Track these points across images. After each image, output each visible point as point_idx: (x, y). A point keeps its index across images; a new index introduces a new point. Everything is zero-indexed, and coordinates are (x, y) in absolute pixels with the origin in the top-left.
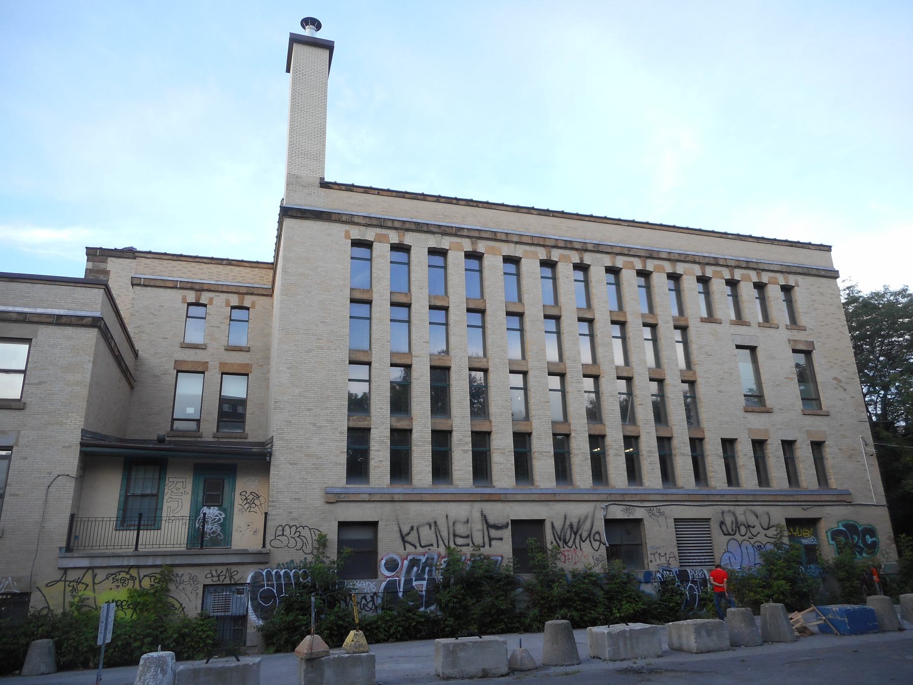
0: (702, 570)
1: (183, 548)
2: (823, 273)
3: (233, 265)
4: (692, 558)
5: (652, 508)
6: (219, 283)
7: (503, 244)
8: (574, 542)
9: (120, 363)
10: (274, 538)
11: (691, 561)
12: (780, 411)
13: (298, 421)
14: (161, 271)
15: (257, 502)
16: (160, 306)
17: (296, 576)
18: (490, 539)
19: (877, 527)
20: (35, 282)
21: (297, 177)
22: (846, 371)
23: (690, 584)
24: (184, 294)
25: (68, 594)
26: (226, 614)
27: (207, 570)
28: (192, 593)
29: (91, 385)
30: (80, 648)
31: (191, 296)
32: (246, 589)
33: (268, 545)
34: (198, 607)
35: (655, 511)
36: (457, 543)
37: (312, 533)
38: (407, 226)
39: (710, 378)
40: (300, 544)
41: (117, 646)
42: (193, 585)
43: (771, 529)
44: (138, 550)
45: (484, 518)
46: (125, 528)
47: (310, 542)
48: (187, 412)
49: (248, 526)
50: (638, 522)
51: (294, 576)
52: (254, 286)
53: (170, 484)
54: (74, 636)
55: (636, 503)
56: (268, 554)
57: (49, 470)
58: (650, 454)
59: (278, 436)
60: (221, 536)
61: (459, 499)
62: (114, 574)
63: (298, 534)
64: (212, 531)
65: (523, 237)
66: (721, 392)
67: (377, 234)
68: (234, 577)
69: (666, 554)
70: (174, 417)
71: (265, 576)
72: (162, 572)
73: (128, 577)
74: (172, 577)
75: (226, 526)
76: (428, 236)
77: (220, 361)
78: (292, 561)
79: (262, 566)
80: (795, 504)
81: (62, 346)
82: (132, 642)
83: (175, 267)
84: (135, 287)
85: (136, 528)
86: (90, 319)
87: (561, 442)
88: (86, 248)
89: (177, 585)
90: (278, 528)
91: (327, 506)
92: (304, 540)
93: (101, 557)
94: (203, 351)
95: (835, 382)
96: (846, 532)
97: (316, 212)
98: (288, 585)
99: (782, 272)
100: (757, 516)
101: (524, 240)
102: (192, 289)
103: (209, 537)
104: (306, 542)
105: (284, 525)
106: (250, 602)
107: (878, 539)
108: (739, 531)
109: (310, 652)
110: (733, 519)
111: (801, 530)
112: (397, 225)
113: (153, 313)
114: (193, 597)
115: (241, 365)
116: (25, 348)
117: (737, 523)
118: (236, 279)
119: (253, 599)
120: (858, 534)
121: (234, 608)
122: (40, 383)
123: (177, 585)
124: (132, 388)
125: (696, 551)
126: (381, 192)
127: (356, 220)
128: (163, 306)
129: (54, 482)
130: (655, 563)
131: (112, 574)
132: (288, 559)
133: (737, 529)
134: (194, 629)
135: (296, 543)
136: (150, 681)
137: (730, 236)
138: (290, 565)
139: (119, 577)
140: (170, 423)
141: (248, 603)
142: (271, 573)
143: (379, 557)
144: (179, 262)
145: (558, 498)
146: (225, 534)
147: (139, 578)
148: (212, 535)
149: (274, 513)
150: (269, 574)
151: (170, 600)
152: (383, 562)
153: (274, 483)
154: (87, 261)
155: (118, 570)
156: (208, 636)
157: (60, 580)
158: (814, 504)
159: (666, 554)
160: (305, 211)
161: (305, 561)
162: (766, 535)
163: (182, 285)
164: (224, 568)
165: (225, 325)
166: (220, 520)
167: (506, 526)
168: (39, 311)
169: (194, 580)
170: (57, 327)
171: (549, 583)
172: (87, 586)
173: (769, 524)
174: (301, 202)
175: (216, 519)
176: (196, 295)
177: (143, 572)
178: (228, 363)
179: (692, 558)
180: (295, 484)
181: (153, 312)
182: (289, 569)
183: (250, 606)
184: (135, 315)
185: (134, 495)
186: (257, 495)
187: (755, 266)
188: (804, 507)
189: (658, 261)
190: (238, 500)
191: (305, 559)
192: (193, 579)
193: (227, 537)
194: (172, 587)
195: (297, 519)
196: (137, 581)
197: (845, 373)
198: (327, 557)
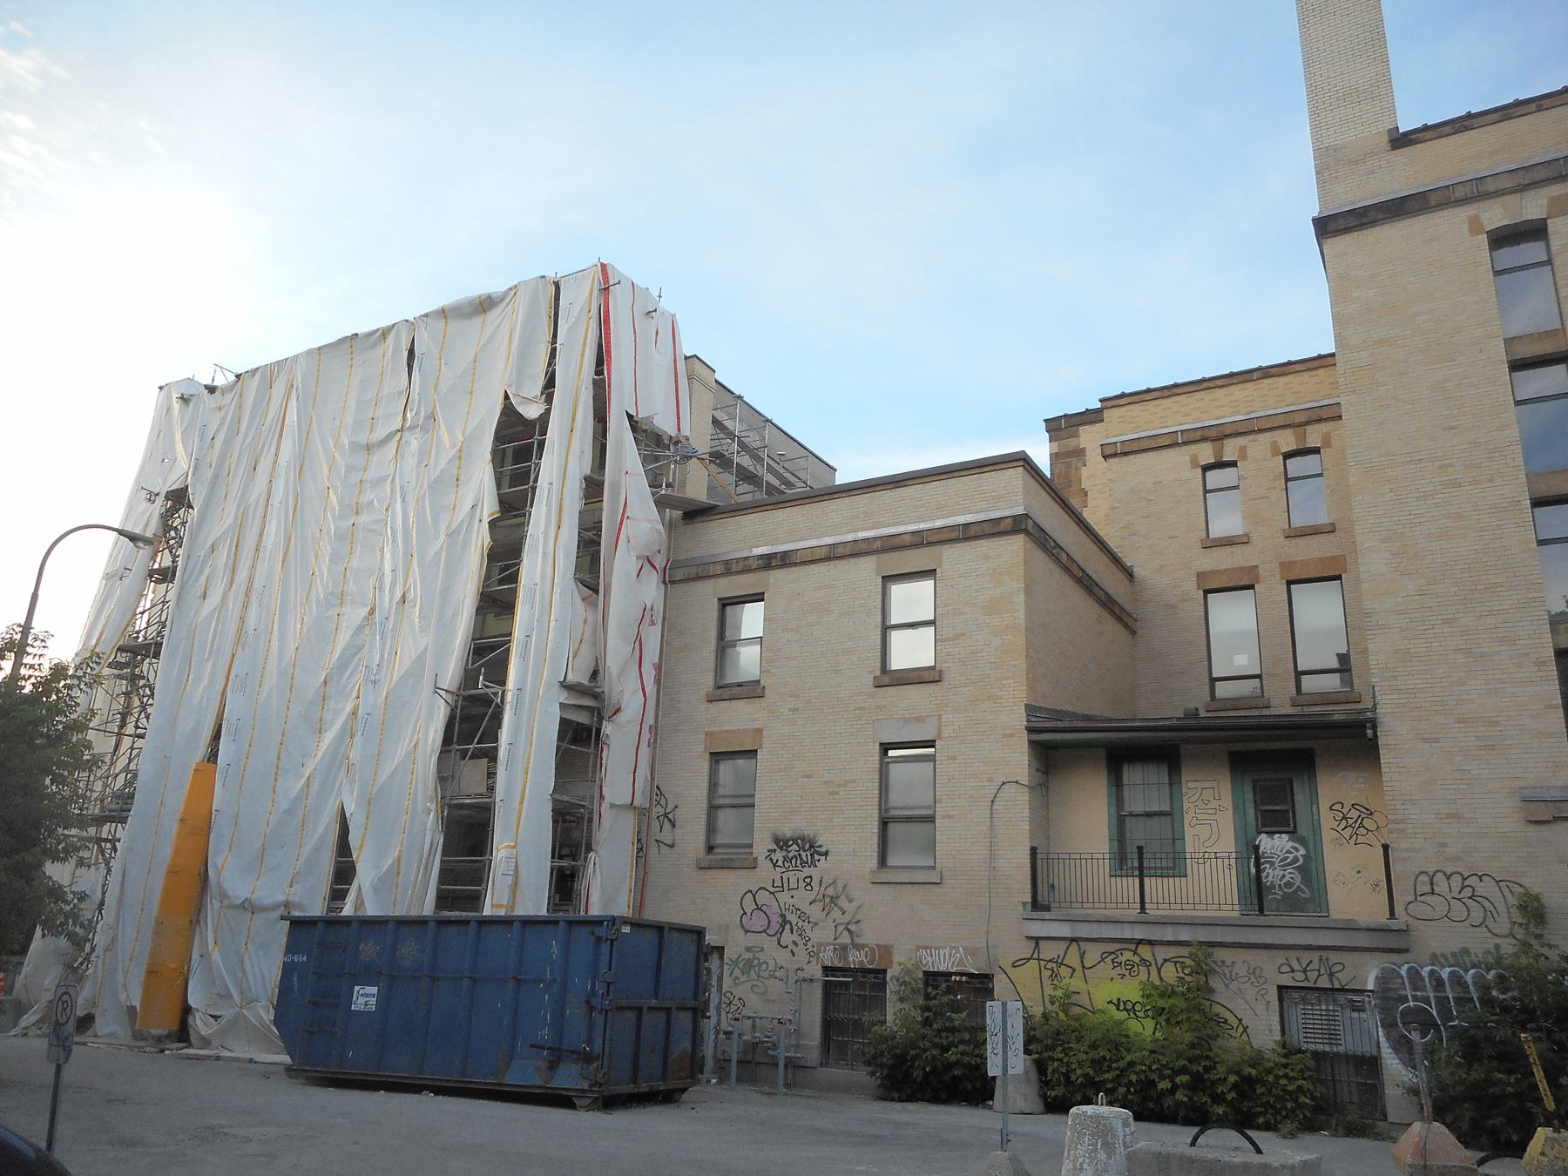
1: (1234, 913)
3: (1272, 376)
6: (1252, 416)
9: (1091, 591)
10: (1412, 898)
13: (1425, 650)
14: (1147, 423)
15: (1367, 823)
16: (1155, 483)
17: (1484, 988)
20: (927, 479)
21: (1335, 151)
24: (1192, 453)
25: (1047, 982)
26: (1335, 1050)
27: (1279, 957)
28: (1256, 1000)
29: (1028, 629)
30: (1073, 1078)
31: (1206, 454)
32: (1370, 1002)
33: (1399, 909)
34: (1274, 1028)
37: (1506, 890)
40: (1477, 915)
41: (1130, 1083)
42: (1256, 984)
44: (1147, 911)
46: (1124, 873)
47: (1502, 908)
48: (1236, 664)
49: (1359, 872)
51: (1475, 984)
52: (1320, 404)
53: (1191, 793)
54: (1061, 1056)
56: (1403, 932)
57: (988, 776)
59: (1387, 683)
60: (1304, 893)
62: (1113, 953)
63: (1467, 892)
64: (1284, 881)
67: (1551, 199)
68: (1338, 975)
70: (1214, 676)
71: (1406, 979)
72: (1191, 956)
73: (1136, 959)
74: (1213, 965)
75: (1311, 870)
77: (1280, 561)
78: (1465, 951)
79: (1395, 957)
81: (978, 573)
82: (1157, 1080)
83: (1169, 408)
84: (1112, 460)
85: (1136, 873)
86: (1010, 520)
88: (1045, 420)
89: (1227, 982)
90: (1420, 878)
91: (1532, 831)
92: (1487, 904)
93: (1171, 923)
94: (1244, 548)
97: (1390, 204)
98: (1463, 1001)
102: (1204, 439)
103: (1281, 893)
104: (1493, 910)
105: (1431, 870)
106: (1380, 1029)
109: (1422, 1163)
113: (1145, 498)
114: (1260, 1008)
115: (1321, 561)
116: (927, 586)
118: (1283, 401)
119: (1389, 1025)
121: (1349, 1038)
122: (957, 637)
123: (1227, 982)
124: (1133, 633)
126: (1546, 103)
127: (1491, 186)
128: (1161, 482)
129: (998, 795)
131: (1111, 953)
132: (1455, 946)
134: (1269, 1071)
135: (1469, 911)
136: (1084, 1161)
138: (1461, 958)
139: (1122, 959)
140: (1208, 686)
141: (1378, 1031)
142: (1417, 972)
144: (1174, 399)
146: (1310, 887)
147: (1156, 964)
148: (1286, 890)
149: (1404, 845)
150: (1414, 974)
151: (1217, 1009)
153: (1392, 783)
154: (1050, 442)
155: (1118, 946)
156: (1300, 1088)
157: (1031, 958)
160: (1366, 210)
161: (1498, 952)
163: (1186, 437)
164: (1315, 956)
165: (1277, 490)
166: (1296, 860)
168: (939, 523)
169: (1257, 975)
170: (967, 543)
172: (1074, 970)
174: (1356, 193)
175: (1287, 857)
176: (1214, 449)
177: (1163, 953)
178: (1296, 562)
180: (1441, 782)
181: (1144, 496)
182: (1460, 967)
183: (1383, 1040)
184: (1117, 508)
185: (1131, 815)
186: (1367, 810)
190: (1328, 821)
191: (1497, 947)
192: (1255, 973)
193: (1317, 895)
194: (1215, 983)
195: (1460, 859)
196: (1153, 969)
198: (1550, 947)
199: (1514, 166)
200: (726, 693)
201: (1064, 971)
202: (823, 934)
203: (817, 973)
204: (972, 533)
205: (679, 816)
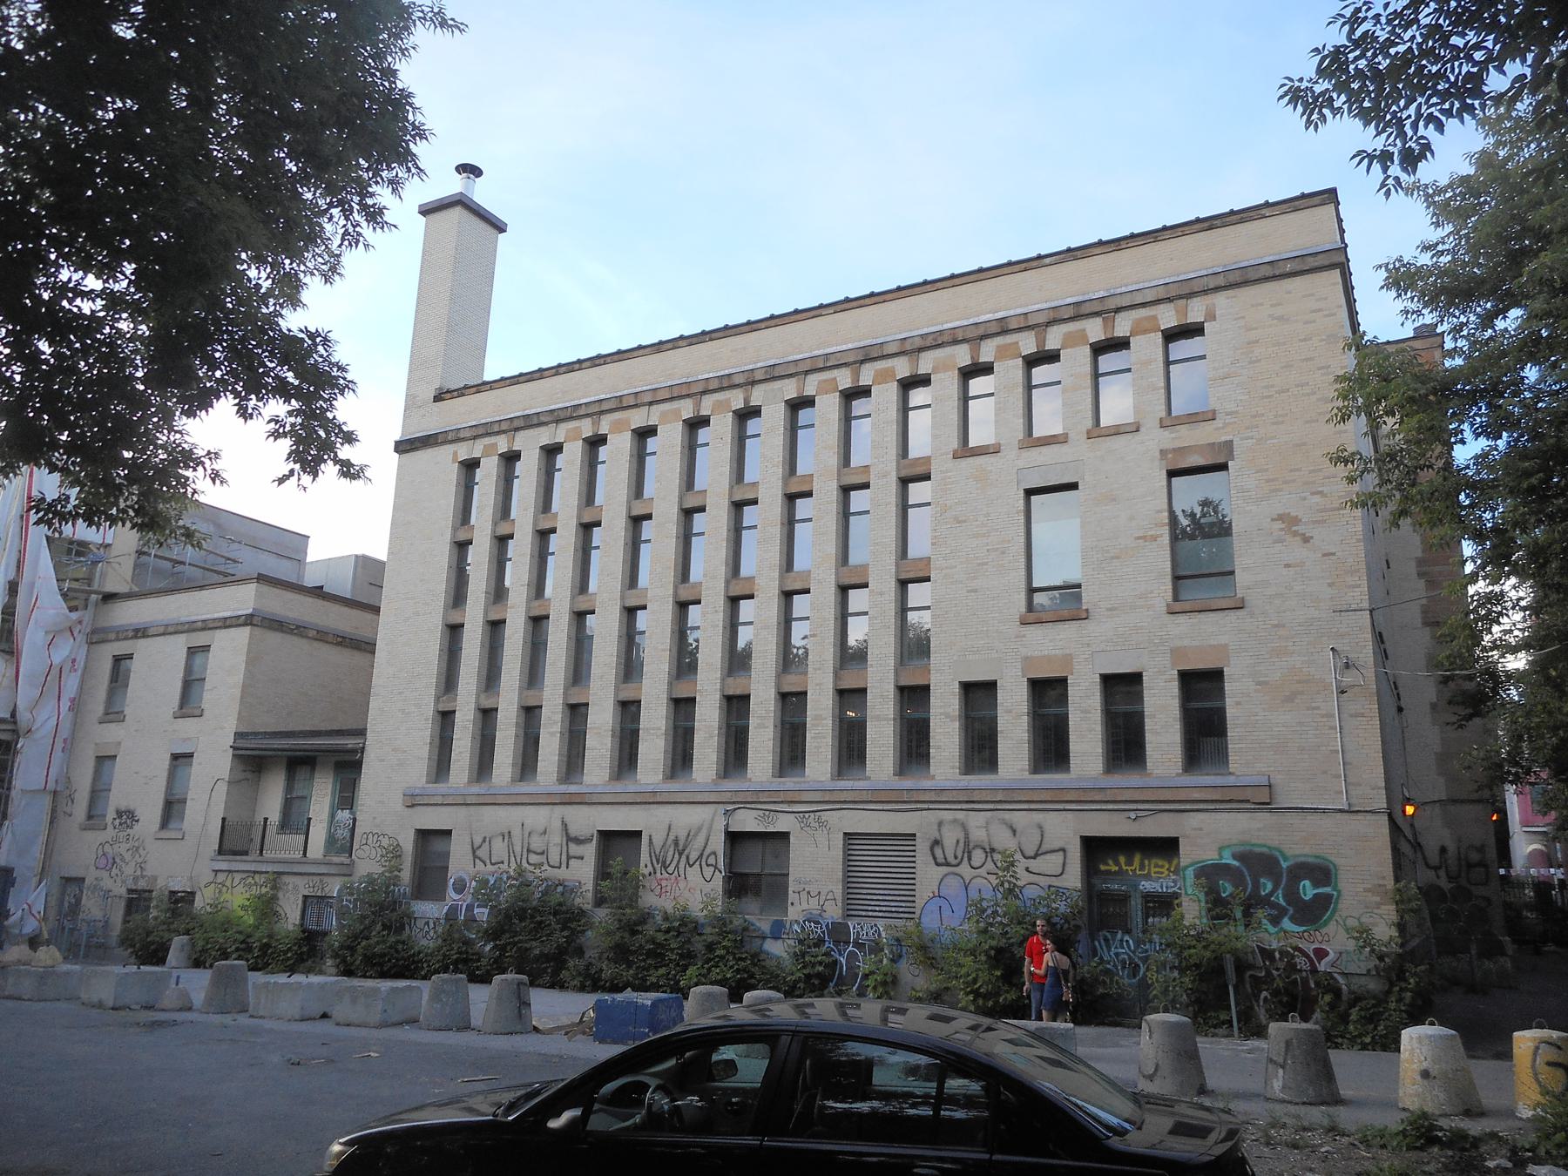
0: (876, 925)
2: (1289, 267)
4: (873, 903)
5: (807, 815)
7: (634, 411)
8: (677, 866)
11: (870, 908)
12: (1110, 613)
18: (569, 858)
19: (1338, 861)
22: (1321, 493)
23: (850, 948)
35: (811, 820)
36: (531, 861)
38: (516, 424)
39: (956, 567)
43: (1048, 857)
45: (565, 826)
50: (784, 836)
55: (781, 805)
58: (816, 722)
61: (1010, 799)
65: (800, 363)
66: (975, 591)
67: (876, 371)
69: (819, 893)
76: (542, 429)
80: (1111, 807)
87: (792, 702)
95: (1279, 525)
96: (1282, 873)
99: (1169, 300)
100: (1014, 832)
101: (661, 395)
107: (1339, 892)
108: (970, 859)
110: (961, 836)
111: (1146, 862)
112: (504, 426)
117: (967, 843)
120: (1276, 877)
125: (881, 892)
126: (494, 385)
127: (1253, 275)
130: (798, 908)
133: (966, 855)
137: (1047, 261)
143: (449, 875)
145: (659, 799)
152: (452, 880)
158: (1163, 807)
159: (819, 893)
162: (1027, 869)
167: (589, 840)
171: (633, 928)
173: (1040, 846)
179: (873, 903)
187: (1097, 307)
188: (1133, 815)
189: (884, 362)
192: (296, 887)
194: (280, 895)
197: (1317, 499)
199: (474, 423)
200: (111, 717)
201: (224, 889)
202: (129, 870)
203: (123, 891)
204: (228, 623)
205: (77, 796)
